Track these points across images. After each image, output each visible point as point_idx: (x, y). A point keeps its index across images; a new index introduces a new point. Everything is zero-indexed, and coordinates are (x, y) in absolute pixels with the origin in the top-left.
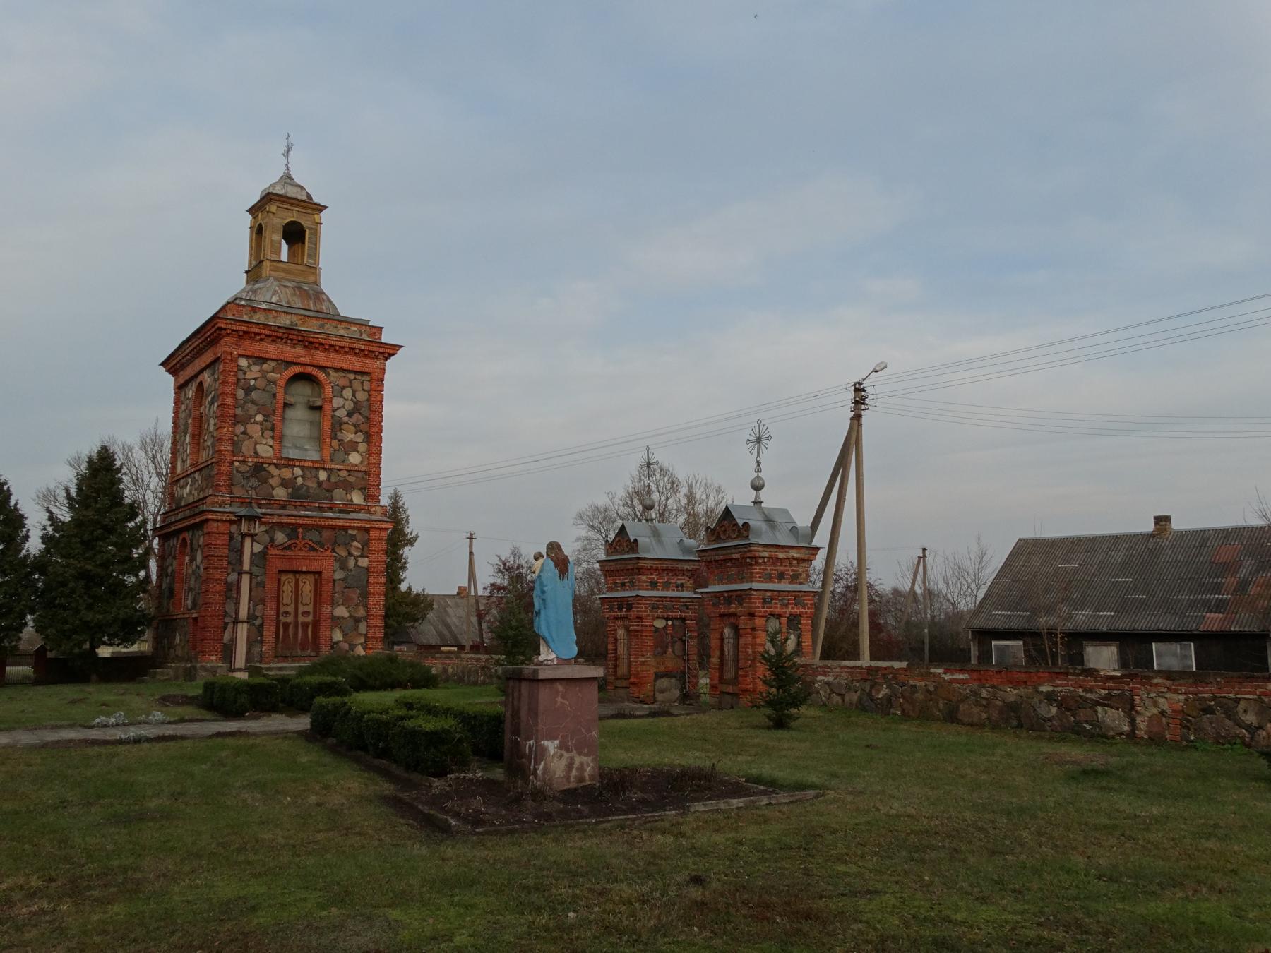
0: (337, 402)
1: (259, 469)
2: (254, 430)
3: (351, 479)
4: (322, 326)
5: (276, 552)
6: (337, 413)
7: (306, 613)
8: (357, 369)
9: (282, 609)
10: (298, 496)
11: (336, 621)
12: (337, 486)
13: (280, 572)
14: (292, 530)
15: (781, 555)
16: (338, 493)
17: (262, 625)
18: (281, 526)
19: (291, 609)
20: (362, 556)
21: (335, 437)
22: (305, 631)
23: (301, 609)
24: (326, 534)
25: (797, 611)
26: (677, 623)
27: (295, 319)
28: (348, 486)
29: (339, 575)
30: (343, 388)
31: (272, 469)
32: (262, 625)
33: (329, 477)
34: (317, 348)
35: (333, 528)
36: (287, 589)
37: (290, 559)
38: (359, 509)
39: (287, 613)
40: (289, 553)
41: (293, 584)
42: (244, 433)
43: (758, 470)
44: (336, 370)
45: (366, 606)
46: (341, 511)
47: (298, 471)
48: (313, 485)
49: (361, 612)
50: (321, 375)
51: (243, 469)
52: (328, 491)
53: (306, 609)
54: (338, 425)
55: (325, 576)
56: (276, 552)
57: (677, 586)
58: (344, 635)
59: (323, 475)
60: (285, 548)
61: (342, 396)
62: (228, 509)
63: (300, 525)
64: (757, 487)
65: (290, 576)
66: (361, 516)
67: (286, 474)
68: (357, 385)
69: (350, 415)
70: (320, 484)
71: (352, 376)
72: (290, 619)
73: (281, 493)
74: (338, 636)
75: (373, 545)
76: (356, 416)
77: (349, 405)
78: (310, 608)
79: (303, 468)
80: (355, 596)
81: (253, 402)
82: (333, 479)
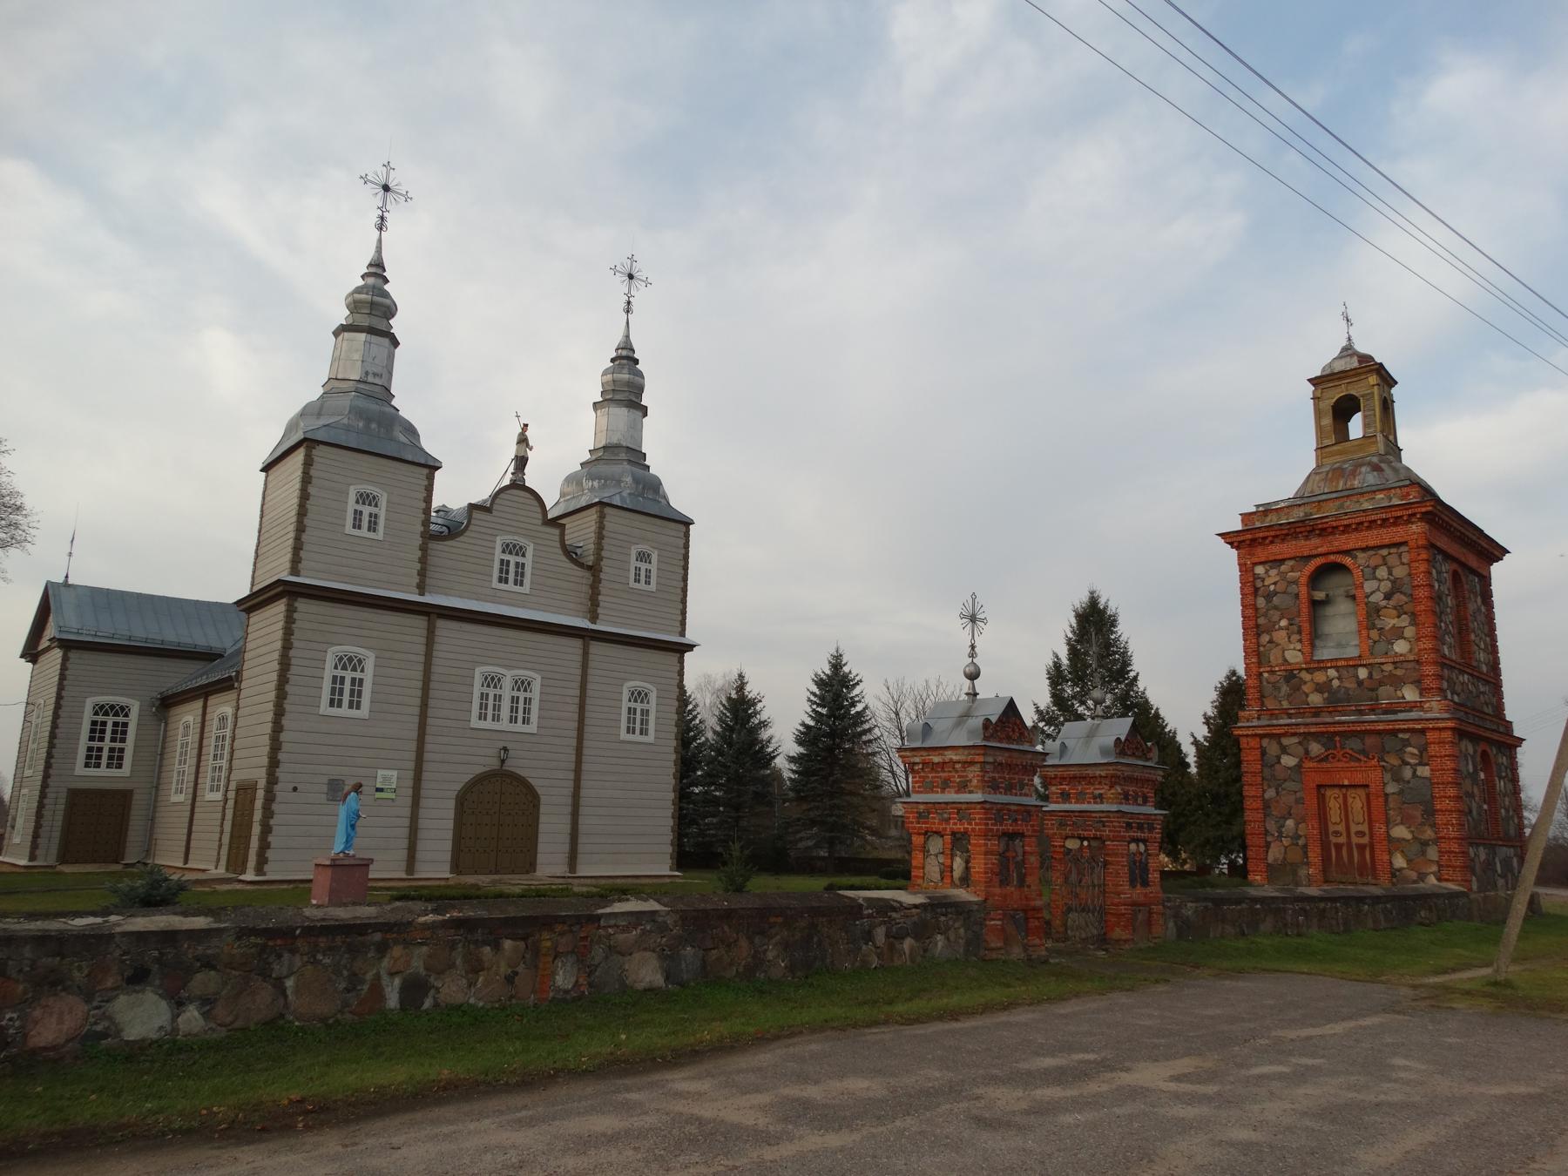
0: (1369, 586)
1: (1290, 676)
2: (1280, 636)
3: (1399, 672)
4: (1342, 507)
5: (1311, 765)
6: (1373, 599)
7: (1361, 834)
8: (1387, 541)
9: (1332, 828)
10: (1336, 701)
11: (1394, 844)
12: (1381, 683)
13: (1319, 786)
14: (1327, 738)
15: (936, 759)
16: (1385, 695)
17: (1305, 846)
18: (1316, 736)
19: (1341, 828)
20: (1421, 764)
21: (1374, 627)
22: (1362, 854)
23: (1354, 828)
24: (1370, 741)
25: (960, 827)
26: (1094, 844)
27: (1308, 509)
28: (1398, 682)
29: (1391, 788)
30: (1376, 567)
31: (1305, 676)
32: (1305, 846)
33: (1370, 674)
34: (1332, 533)
35: (1379, 732)
36: (1334, 806)
37: (1328, 771)
38: (1412, 706)
39: (1337, 833)
40: (1324, 765)
41: (1341, 800)
42: (1271, 641)
43: (973, 655)
44: (1364, 550)
45: (1433, 825)
46: (1386, 712)
47: (1332, 673)
48: (1351, 685)
49: (1429, 833)
50: (1348, 561)
51: (1272, 679)
52: (1372, 690)
53: (1360, 828)
54: (1374, 612)
55: (1372, 790)
56: (1311, 765)
57: (1095, 798)
58: (1409, 861)
59: (1363, 673)
60: (1322, 760)
61: (1375, 578)
62: (1256, 723)
63: (1336, 733)
64: (973, 676)
65: (1336, 791)
66: (1414, 715)
67: (1320, 677)
68: (1392, 560)
69: (1388, 597)
70: (1360, 683)
71: (1384, 552)
72: (1342, 840)
73: (1316, 699)
74: (1399, 862)
75: (1433, 749)
76: (1397, 596)
77: (1386, 586)
78: (1365, 828)
79: (1337, 668)
80: (1417, 813)
81: (1276, 608)
82: (1376, 676)
